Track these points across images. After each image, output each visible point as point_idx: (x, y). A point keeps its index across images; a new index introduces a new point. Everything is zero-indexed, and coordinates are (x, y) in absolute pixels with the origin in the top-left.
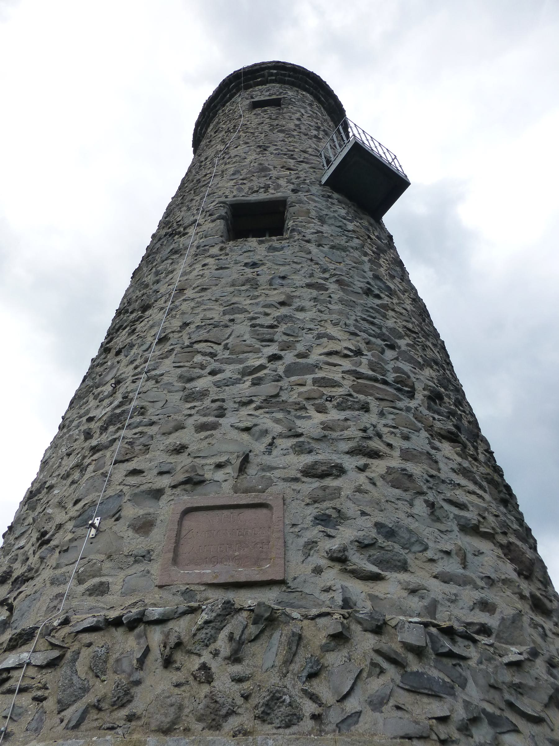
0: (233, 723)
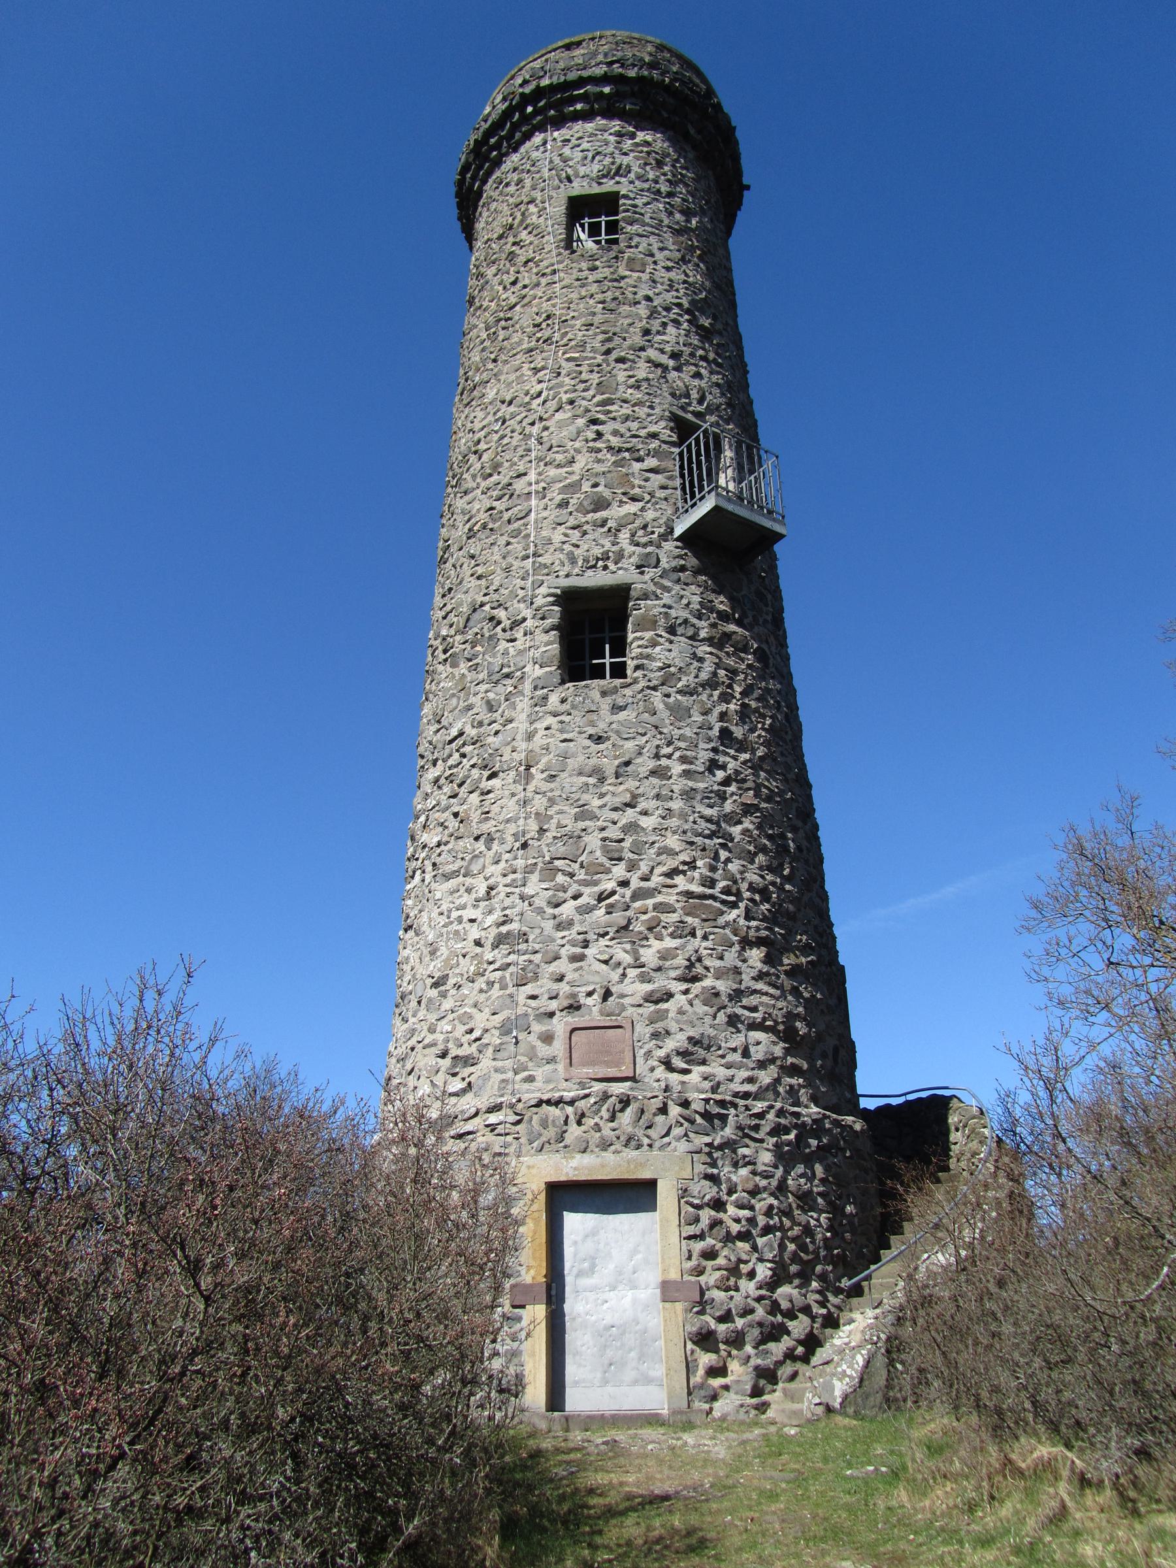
0: (613, 1148)
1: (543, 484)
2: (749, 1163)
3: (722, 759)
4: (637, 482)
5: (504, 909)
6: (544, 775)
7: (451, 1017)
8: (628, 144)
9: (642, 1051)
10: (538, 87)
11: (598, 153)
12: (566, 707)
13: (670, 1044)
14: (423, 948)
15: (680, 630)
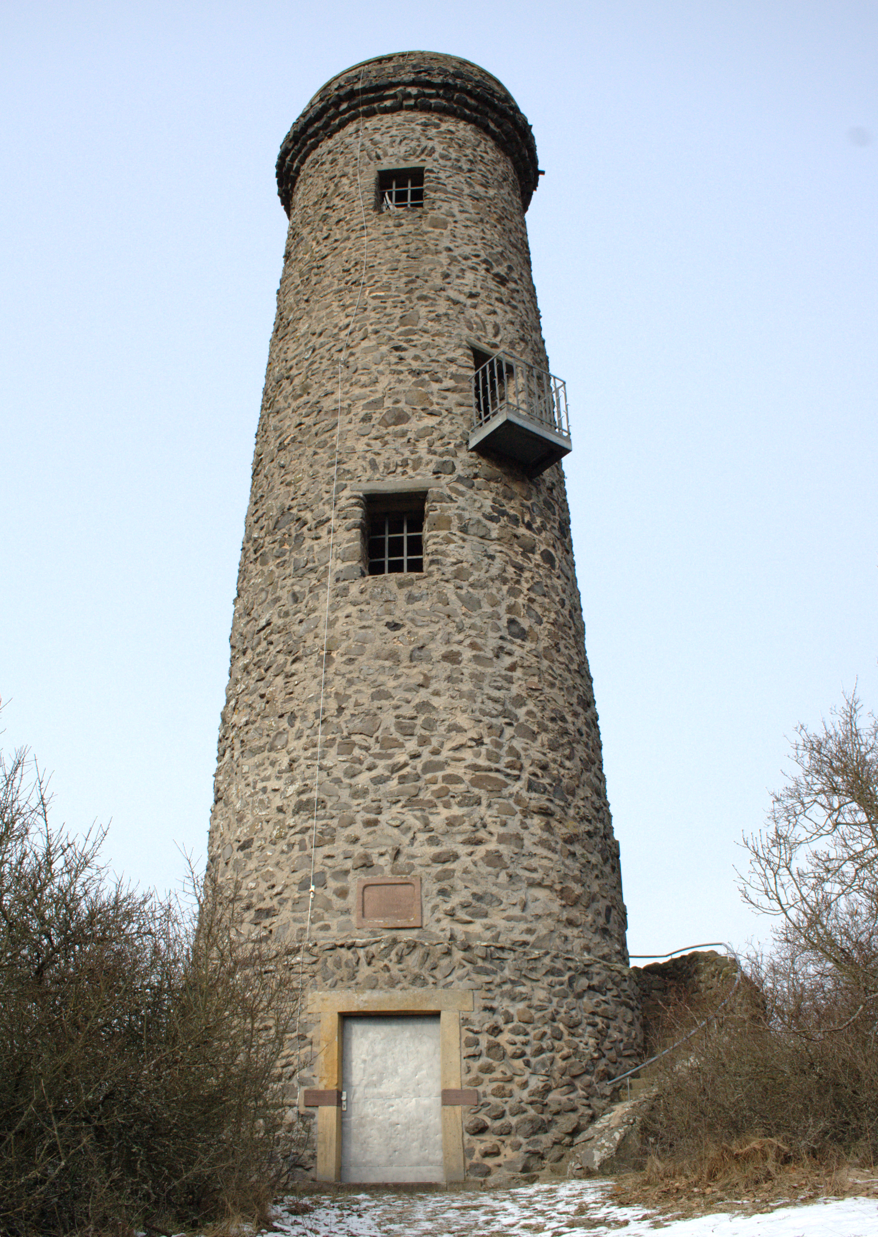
0: (400, 986)
1: (349, 402)
2: (525, 999)
3: (508, 646)
4: (435, 400)
5: (304, 779)
6: (344, 659)
7: (255, 875)
8: (432, 132)
9: (430, 905)
10: (352, 90)
11: (405, 139)
12: (366, 596)
13: (455, 900)
14: (231, 817)
15: (472, 530)
